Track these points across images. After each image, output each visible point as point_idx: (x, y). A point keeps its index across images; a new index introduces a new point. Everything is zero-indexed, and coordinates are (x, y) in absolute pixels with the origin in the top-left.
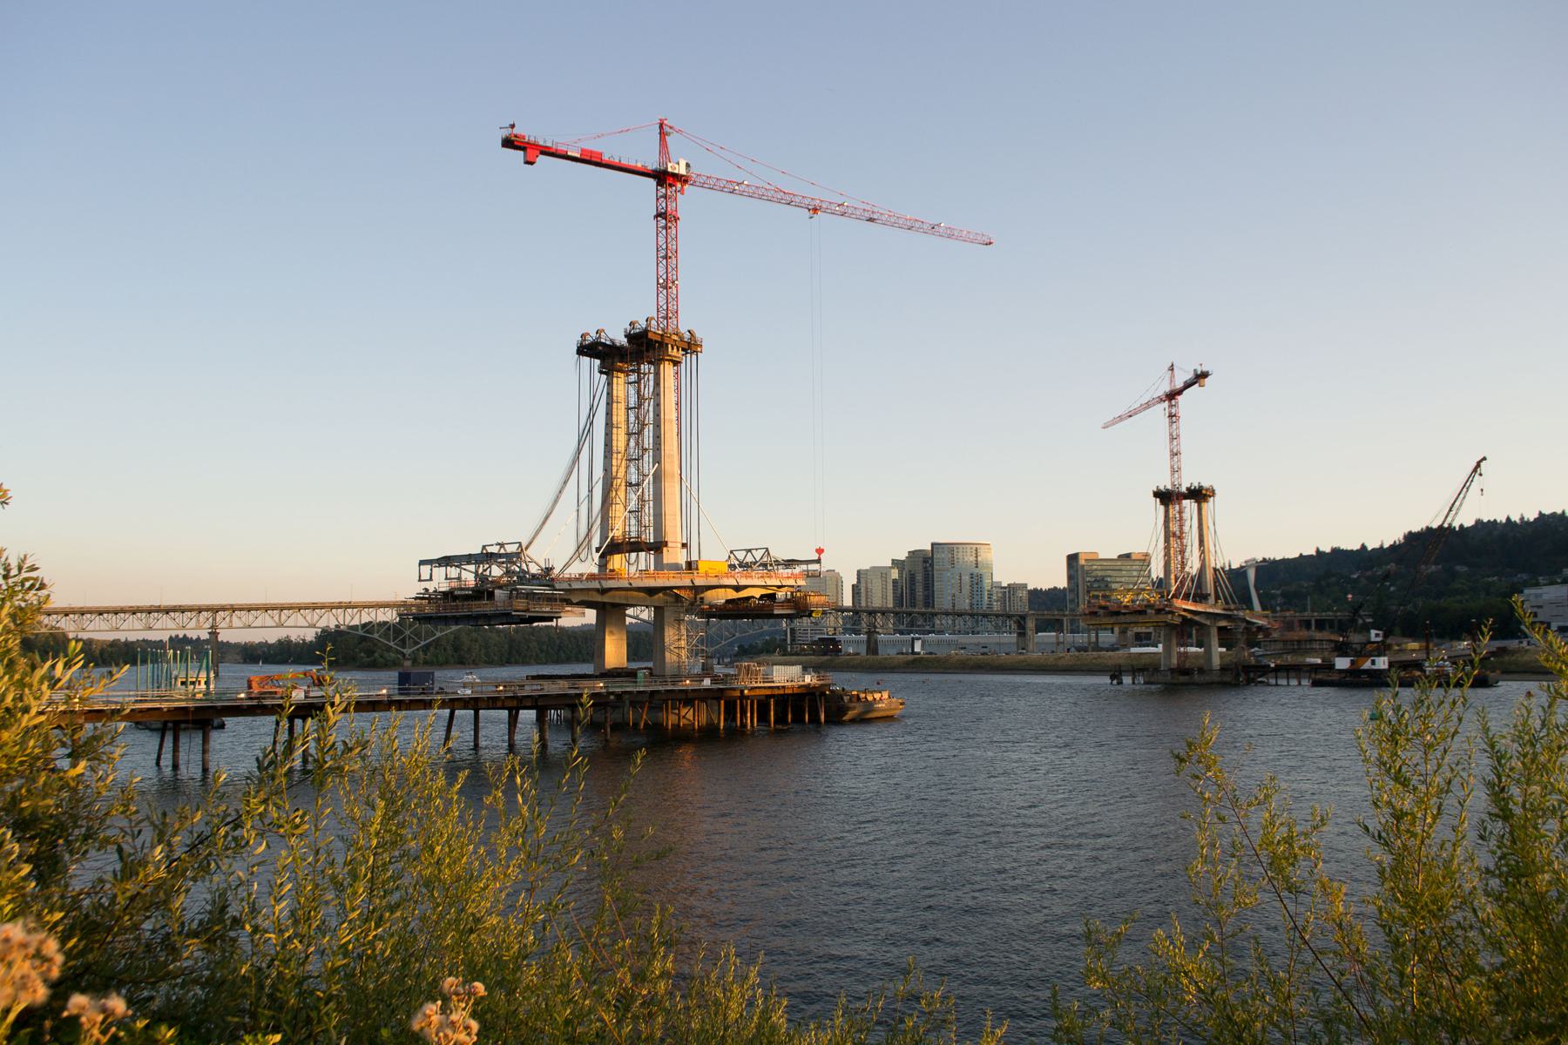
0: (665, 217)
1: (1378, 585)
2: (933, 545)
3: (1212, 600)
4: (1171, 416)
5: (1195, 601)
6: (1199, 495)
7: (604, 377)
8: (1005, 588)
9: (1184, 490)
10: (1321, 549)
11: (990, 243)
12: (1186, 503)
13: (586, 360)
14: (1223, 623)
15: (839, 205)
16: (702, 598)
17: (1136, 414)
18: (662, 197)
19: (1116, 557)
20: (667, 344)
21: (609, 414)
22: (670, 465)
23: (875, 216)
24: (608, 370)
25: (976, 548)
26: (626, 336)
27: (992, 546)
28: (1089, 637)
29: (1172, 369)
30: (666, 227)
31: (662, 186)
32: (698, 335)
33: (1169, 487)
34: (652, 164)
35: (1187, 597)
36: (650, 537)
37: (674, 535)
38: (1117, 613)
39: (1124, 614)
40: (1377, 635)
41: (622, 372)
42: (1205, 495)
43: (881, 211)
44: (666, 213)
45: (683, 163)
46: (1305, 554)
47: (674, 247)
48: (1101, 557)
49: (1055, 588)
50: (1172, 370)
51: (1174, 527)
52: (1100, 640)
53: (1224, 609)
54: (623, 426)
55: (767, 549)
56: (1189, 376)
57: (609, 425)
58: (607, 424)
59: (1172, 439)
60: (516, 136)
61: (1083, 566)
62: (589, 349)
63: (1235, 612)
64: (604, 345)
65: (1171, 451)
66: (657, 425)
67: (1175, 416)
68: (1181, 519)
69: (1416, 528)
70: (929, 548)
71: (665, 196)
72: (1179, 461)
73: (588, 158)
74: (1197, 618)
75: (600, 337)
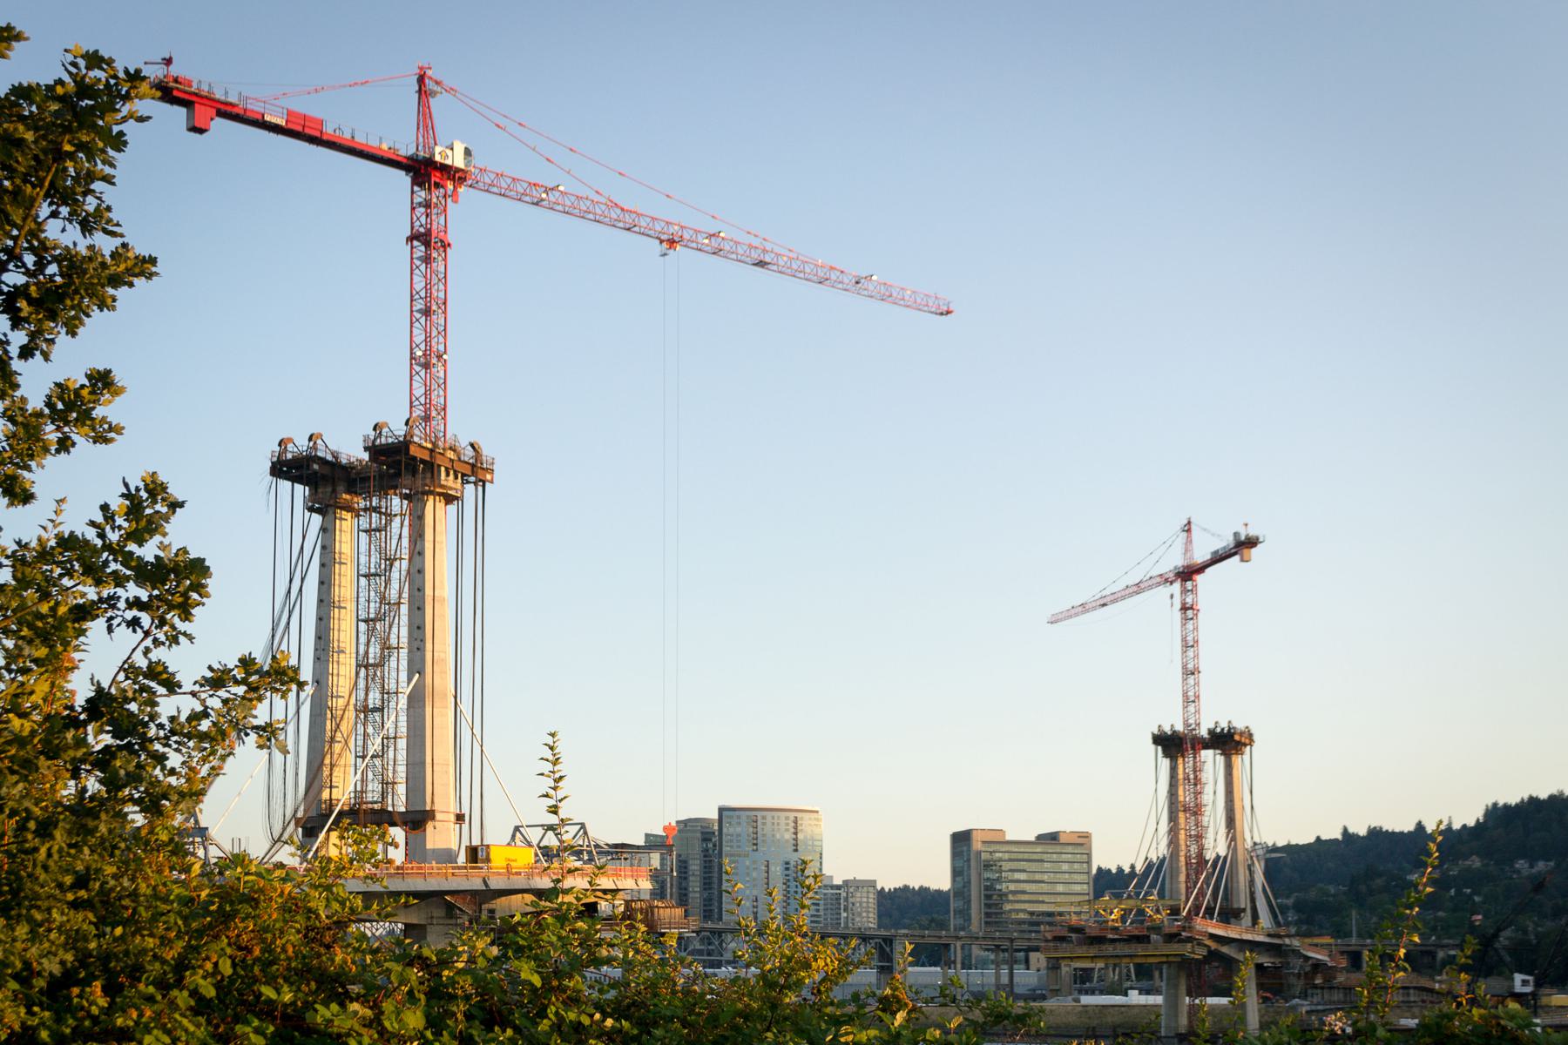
0: (426, 241)
1: (1453, 892)
2: (721, 810)
3: (1247, 919)
4: (1184, 608)
5: (1222, 921)
6: (1228, 742)
7: (317, 519)
8: (838, 887)
9: (1204, 733)
10: (1351, 830)
11: (948, 312)
12: (1207, 755)
13: (285, 485)
14: (1266, 960)
15: (711, 236)
16: (492, 911)
17: (1115, 601)
18: (420, 204)
19: (1032, 838)
20: (439, 466)
21: (325, 583)
22: (441, 678)
23: (767, 259)
24: (323, 505)
25: (795, 817)
26: (366, 449)
27: (822, 815)
28: (998, 976)
29: (1188, 528)
30: (427, 260)
31: (421, 185)
32: (486, 452)
33: (1180, 727)
34: (406, 146)
35: (1209, 912)
36: (399, 802)
37: (443, 801)
38: (1099, 940)
39: (1113, 941)
40: (1525, 983)
41: (349, 508)
42: (1239, 743)
43: (777, 249)
44: (428, 232)
45: (459, 148)
46: (1324, 837)
47: (442, 295)
48: (1009, 837)
49: (906, 888)
50: (1189, 531)
51: (1184, 795)
52: (1016, 980)
53: (1269, 935)
54: (351, 606)
55: (583, 826)
56: (1227, 541)
57: (326, 602)
58: (320, 601)
59: (1186, 646)
60: (176, 80)
61: (979, 853)
62: (288, 468)
63: (1287, 941)
64: (323, 461)
65: (1185, 667)
66: (417, 608)
67: (1191, 608)
68: (1197, 781)
69: (1513, 798)
70: (715, 816)
71: (427, 205)
72: (1197, 684)
73: (300, 129)
74: (1225, 950)
75: (315, 448)
